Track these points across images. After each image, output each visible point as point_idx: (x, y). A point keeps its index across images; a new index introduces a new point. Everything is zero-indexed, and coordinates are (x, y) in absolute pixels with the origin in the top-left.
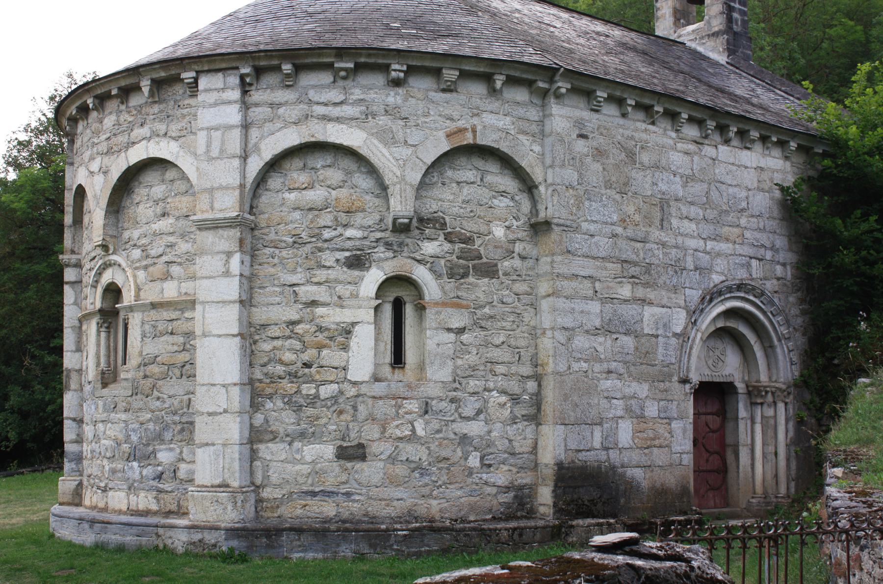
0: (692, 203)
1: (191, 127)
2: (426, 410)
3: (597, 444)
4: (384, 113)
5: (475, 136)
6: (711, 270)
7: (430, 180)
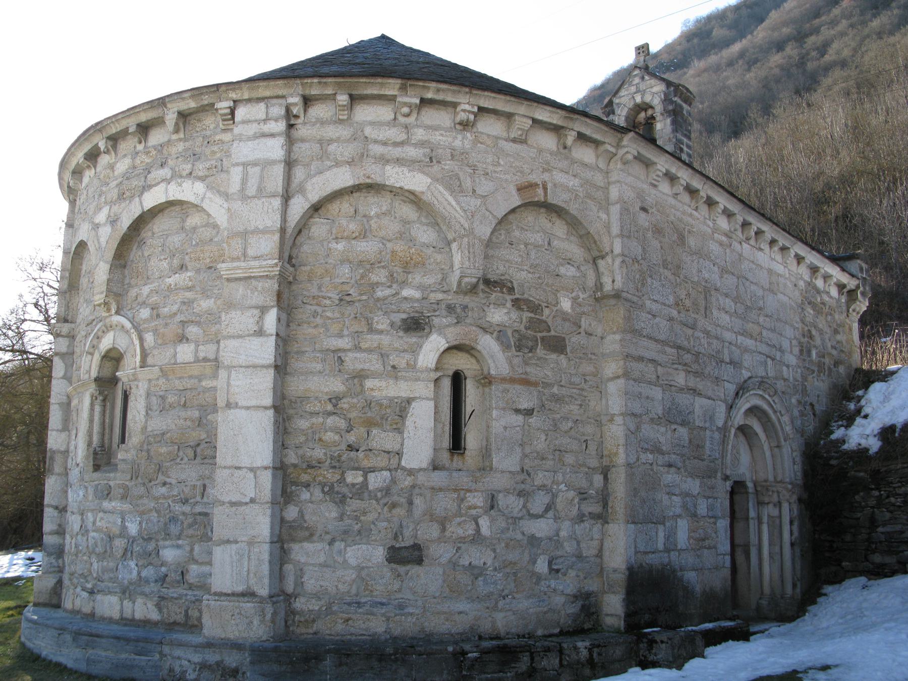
0: (727, 295)
1: (222, 165)
2: (492, 504)
3: (661, 546)
4: (450, 158)
7: (497, 238)
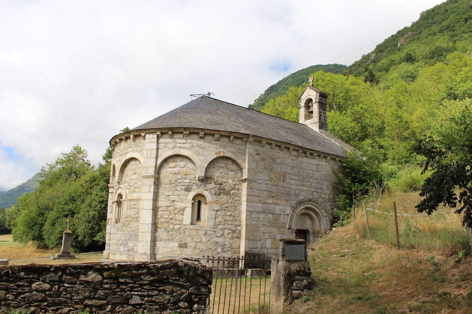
0: (294, 175)
5: (224, 154)
6: (299, 195)
